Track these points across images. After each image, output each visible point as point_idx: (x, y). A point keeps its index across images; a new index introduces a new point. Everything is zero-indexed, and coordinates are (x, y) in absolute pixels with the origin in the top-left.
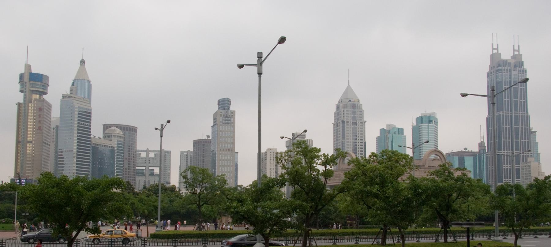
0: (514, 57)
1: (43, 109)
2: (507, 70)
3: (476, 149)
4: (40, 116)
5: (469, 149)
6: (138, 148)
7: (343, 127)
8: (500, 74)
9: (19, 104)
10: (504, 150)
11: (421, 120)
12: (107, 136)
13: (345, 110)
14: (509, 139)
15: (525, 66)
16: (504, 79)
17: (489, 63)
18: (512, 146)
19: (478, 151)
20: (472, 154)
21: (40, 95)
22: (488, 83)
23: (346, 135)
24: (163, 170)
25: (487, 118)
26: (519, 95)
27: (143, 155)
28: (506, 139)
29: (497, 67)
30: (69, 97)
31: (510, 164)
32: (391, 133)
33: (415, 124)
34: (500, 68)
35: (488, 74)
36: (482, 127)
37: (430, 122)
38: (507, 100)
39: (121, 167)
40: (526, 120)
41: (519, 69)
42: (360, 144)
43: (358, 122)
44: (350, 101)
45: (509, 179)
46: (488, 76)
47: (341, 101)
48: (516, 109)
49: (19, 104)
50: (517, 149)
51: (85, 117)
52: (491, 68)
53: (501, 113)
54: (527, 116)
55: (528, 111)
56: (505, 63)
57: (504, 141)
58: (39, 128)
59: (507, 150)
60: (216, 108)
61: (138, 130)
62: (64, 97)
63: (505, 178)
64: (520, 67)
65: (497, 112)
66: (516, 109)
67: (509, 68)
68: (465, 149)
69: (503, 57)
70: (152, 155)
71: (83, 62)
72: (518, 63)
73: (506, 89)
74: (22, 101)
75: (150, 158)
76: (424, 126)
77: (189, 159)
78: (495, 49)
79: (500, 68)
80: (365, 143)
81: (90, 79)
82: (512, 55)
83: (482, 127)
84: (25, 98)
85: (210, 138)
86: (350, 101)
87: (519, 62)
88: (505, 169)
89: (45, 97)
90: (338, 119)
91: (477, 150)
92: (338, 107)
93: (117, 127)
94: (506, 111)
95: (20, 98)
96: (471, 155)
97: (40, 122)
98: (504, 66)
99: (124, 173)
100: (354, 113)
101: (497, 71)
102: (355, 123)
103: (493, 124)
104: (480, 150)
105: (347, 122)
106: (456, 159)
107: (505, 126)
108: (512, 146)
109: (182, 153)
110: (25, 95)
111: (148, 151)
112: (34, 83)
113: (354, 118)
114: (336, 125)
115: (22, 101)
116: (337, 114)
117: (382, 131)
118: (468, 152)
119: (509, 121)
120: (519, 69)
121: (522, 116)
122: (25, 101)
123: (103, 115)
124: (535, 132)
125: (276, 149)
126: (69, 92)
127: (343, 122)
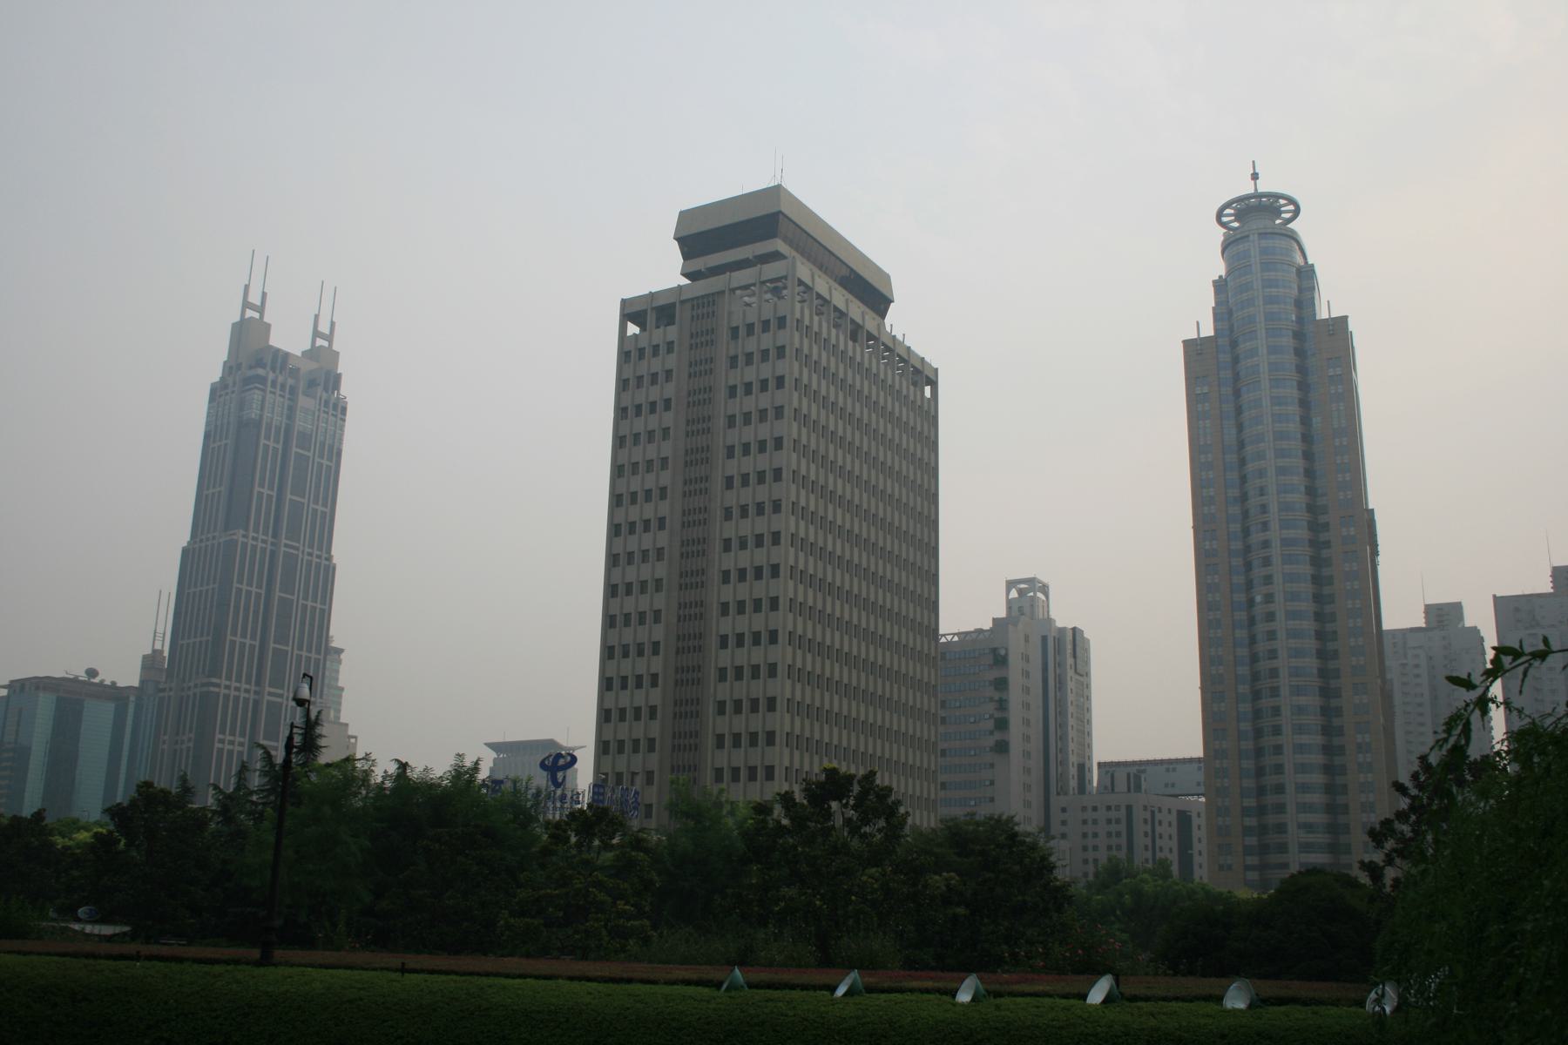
0: (312, 353)
2: (283, 386)
5: (106, 676)
10: (229, 678)
14: (253, 637)
15: (345, 389)
16: (267, 414)
17: (223, 355)
19: (136, 684)
20: (115, 694)
22: (208, 424)
25: (185, 552)
28: (309, 651)
29: (251, 367)
31: (243, 734)
34: (261, 371)
38: (266, 491)
41: (325, 396)
45: (238, 739)
46: (212, 400)
52: (230, 368)
54: (323, 611)
55: (333, 552)
56: (280, 359)
59: (239, 680)
63: (223, 732)
67: (290, 382)
68: (92, 673)
69: (278, 340)
72: (319, 380)
79: (261, 371)
88: (220, 751)
91: (134, 681)
94: (256, 530)
98: (273, 369)
101: (247, 381)
104: (142, 682)
107: (238, 639)
119: (250, 667)
121: (309, 563)
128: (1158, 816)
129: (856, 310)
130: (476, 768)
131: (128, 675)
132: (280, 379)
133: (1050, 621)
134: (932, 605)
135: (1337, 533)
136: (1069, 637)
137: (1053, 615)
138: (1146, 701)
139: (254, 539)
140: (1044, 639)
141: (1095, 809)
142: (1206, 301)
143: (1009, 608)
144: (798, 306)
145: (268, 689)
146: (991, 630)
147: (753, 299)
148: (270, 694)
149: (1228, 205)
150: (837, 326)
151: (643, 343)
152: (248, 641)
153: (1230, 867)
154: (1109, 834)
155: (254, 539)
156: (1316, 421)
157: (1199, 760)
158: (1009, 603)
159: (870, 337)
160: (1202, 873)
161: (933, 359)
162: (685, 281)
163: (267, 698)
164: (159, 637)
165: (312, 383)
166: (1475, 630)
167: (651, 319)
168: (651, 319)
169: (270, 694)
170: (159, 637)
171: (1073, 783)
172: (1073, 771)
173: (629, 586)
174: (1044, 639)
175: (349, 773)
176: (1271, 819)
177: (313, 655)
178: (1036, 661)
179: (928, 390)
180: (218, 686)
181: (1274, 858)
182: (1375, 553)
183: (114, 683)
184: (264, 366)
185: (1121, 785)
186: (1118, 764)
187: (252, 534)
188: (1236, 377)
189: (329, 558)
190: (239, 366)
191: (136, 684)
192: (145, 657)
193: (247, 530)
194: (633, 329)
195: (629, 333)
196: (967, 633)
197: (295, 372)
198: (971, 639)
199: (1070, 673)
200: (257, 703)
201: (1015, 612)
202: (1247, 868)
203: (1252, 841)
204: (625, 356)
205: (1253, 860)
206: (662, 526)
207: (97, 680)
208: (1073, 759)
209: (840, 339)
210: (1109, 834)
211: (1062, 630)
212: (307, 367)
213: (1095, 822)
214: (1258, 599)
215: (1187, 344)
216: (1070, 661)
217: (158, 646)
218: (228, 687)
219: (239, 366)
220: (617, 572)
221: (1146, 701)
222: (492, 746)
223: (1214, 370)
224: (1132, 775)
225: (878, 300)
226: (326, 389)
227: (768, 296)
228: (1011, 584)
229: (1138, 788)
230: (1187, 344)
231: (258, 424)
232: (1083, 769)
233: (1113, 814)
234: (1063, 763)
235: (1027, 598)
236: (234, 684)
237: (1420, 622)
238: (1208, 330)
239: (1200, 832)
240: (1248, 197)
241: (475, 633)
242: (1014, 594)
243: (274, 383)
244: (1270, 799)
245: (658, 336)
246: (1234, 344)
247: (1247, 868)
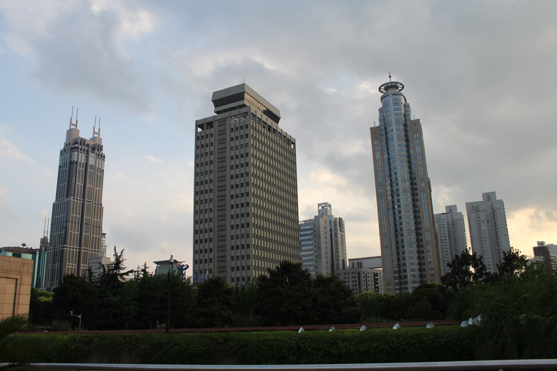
0: (93, 139)
2: (84, 150)
5: (29, 246)
8: (76, 153)
15: (104, 151)
20: (32, 252)
25: (54, 204)
29: (73, 144)
34: (77, 145)
36: (47, 219)
41: (98, 153)
45: (74, 264)
46: (61, 155)
52: (66, 145)
56: (83, 142)
65: (67, 196)
67: (86, 148)
68: (24, 245)
69: (82, 135)
72: (96, 148)
78: (73, 125)
79: (77, 145)
82: (92, 137)
83: (47, 219)
87: (99, 145)
96: (30, 253)
98: (81, 144)
101: (73, 149)
103: (60, 210)
104: (41, 247)
120: (98, 153)
124: (105, 234)
128: (368, 275)
129: (270, 122)
131: (36, 245)
132: (83, 148)
133: (332, 216)
134: (297, 213)
135: (419, 187)
136: (338, 221)
137: (333, 214)
138: (363, 241)
139: (77, 199)
140: (330, 221)
141: (348, 274)
142: (377, 115)
143: (319, 212)
144: (252, 121)
145: (83, 248)
146: (314, 219)
147: (238, 119)
148: (83, 266)
149: (382, 86)
150: (264, 127)
151: (203, 134)
153: (390, 289)
154: (353, 281)
155: (77, 199)
156: (412, 152)
157: (379, 257)
158: (319, 210)
159: (274, 130)
160: (382, 292)
161: (294, 137)
162: (216, 114)
163: (83, 250)
164: (46, 233)
165: (94, 149)
166: (461, 213)
167: (205, 126)
168: (205, 126)
169: (83, 266)
170: (46, 233)
171: (341, 266)
172: (341, 262)
173: (201, 241)
174: (330, 221)
175: (112, 274)
176: (404, 286)
178: (330, 228)
179: (292, 145)
180: (67, 247)
181: (404, 286)
182: (430, 191)
183: (31, 248)
184: (78, 144)
185: (356, 266)
186: (355, 259)
187: (76, 198)
188: (387, 138)
189: (101, 205)
190: (70, 144)
191: (39, 248)
192: (41, 239)
193: (74, 196)
194: (199, 130)
195: (199, 131)
196: (307, 221)
197: (88, 145)
198: (307, 222)
199: (339, 232)
200: (80, 253)
201: (321, 214)
202: (396, 289)
203: (397, 281)
204: (197, 138)
205: (397, 287)
206: (211, 221)
208: (341, 258)
209: (266, 131)
210: (353, 277)
211: (336, 219)
212: (91, 143)
213: (348, 278)
214: (396, 207)
215: (372, 129)
216: (339, 228)
217: (46, 235)
218: (70, 248)
219: (70, 144)
220: (197, 216)
221: (363, 241)
222: (157, 263)
223: (380, 135)
224: (358, 263)
225: (276, 119)
226: (98, 150)
227: (242, 118)
228: (319, 205)
229: (361, 267)
230: (372, 129)
231: (77, 163)
232: (344, 261)
233: (354, 275)
234: (338, 260)
235: (324, 208)
236: (72, 247)
238: (377, 124)
239: (380, 278)
240: (388, 83)
241: (151, 219)
242: (320, 208)
243: (81, 149)
244: (403, 280)
245: (208, 132)
246: (386, 128)
247: (396, 289)
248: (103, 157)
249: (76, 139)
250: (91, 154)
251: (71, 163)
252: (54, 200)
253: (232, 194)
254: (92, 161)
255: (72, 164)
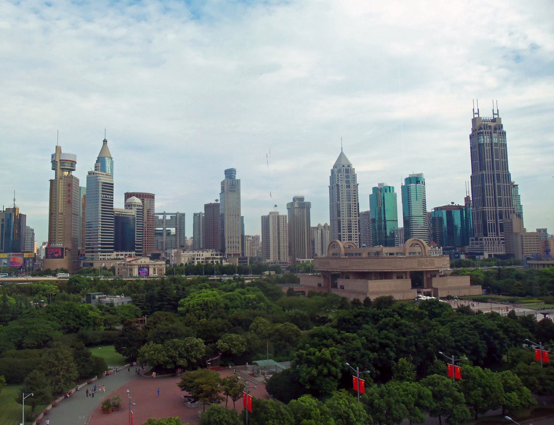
1: (71, 183)
3: (463, 204)
4: (69, 191)
5: (456, 203)
6: (156, 212)
7: (338, 189)
8: (482, 137)
9: (51, 181)
11: (409, 180)
12: (128, 206)
13: (340, 174)
18: (494, 191)
20: (459, 208)
21: (69, 172)
23: (342, 228)
24: (178, 230)
25: (471, 177)
26: (500, 155)
27: (161, 217)
30: (94, 173)
32: (383, 190)
33: (404, 185)
34: (481, 131)
35: (470, 136)
37: (418, 182)
39: (140, 234)
40: (509, 176)
42: (355, 236)
43: (352, 185)
44: (343, 166)
47: (335, 166)
48: (499, 181)
49: (51, 181)
50: (500, 205)
51: (109, 188)
52: (474, 130)
53: (484, 172)
57: (487, 198)
58: (69, 202)
60: (223, 177)
61: (155, 197)
62: (90, 173)
64: (499, 129)
65: (481, 170)
66: (498, 169)
67: (489, 131)
68: (453, 203)
70: (168, 217)
71: (105, 141)
73: (487, 143)
74: (54, 178)
75: (167, 220)
76: (413, 186)
77: (201, 219)
79: (481, 131)
80: (358, 204)
81: (112, 157)
84: (56, 175)
85: (219, 202)
86: (343, 166)
87: (499, 125)
89: (73, 173)
90: (333, 183)
92: (332, 172)
93: (137, 197)
95: (52, 175)
96: (458, 209)
97: (69, 196)
99: (144, 242)
100: (347, 177)
101: (479, 134)
102: (348, 187)
105: (342, 185)
106: (444, 212)
108: (494, 191)
109: (195, 215)
110: (56, 173)
111: (164, 214)
112: (62, 164)
113: (348, 182)
114: (331, 188)
115: (54, 178)
116: (332, 178)
117: (375, 189)
118: (455, 206)
122: (56, 178)
123: (125, 182)
124: (517, 185)
125: (278, 212)
126: (93, 169)
127: (338, 185)
130: (300, 207)
152: (491, 197)
177: (508, 197)
189: (508, 172)
207: (454, 205)
237: (536, 231)
238: (527, 231)
248: (504, 134)
249: (480, 125)
250: (494, 135)
251: (480, 145)
252: (471, 174)
253: (468, 283)
254: (495, 140)
255: (480, 145)
